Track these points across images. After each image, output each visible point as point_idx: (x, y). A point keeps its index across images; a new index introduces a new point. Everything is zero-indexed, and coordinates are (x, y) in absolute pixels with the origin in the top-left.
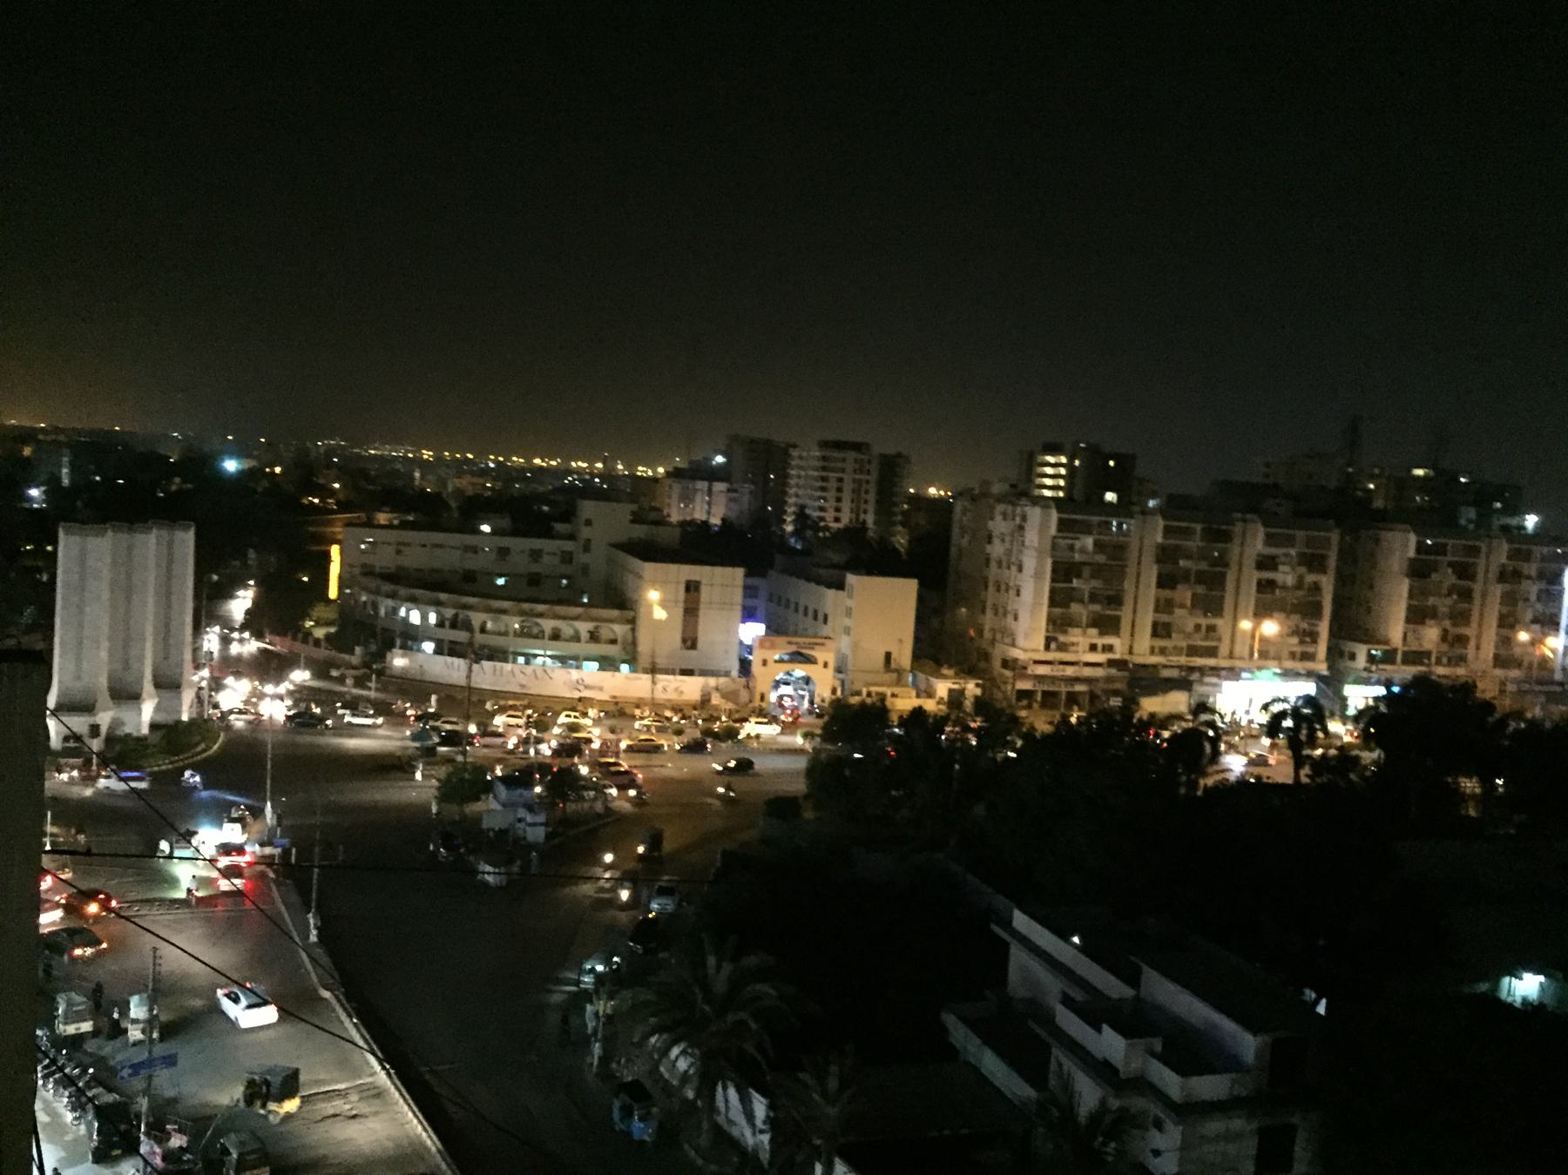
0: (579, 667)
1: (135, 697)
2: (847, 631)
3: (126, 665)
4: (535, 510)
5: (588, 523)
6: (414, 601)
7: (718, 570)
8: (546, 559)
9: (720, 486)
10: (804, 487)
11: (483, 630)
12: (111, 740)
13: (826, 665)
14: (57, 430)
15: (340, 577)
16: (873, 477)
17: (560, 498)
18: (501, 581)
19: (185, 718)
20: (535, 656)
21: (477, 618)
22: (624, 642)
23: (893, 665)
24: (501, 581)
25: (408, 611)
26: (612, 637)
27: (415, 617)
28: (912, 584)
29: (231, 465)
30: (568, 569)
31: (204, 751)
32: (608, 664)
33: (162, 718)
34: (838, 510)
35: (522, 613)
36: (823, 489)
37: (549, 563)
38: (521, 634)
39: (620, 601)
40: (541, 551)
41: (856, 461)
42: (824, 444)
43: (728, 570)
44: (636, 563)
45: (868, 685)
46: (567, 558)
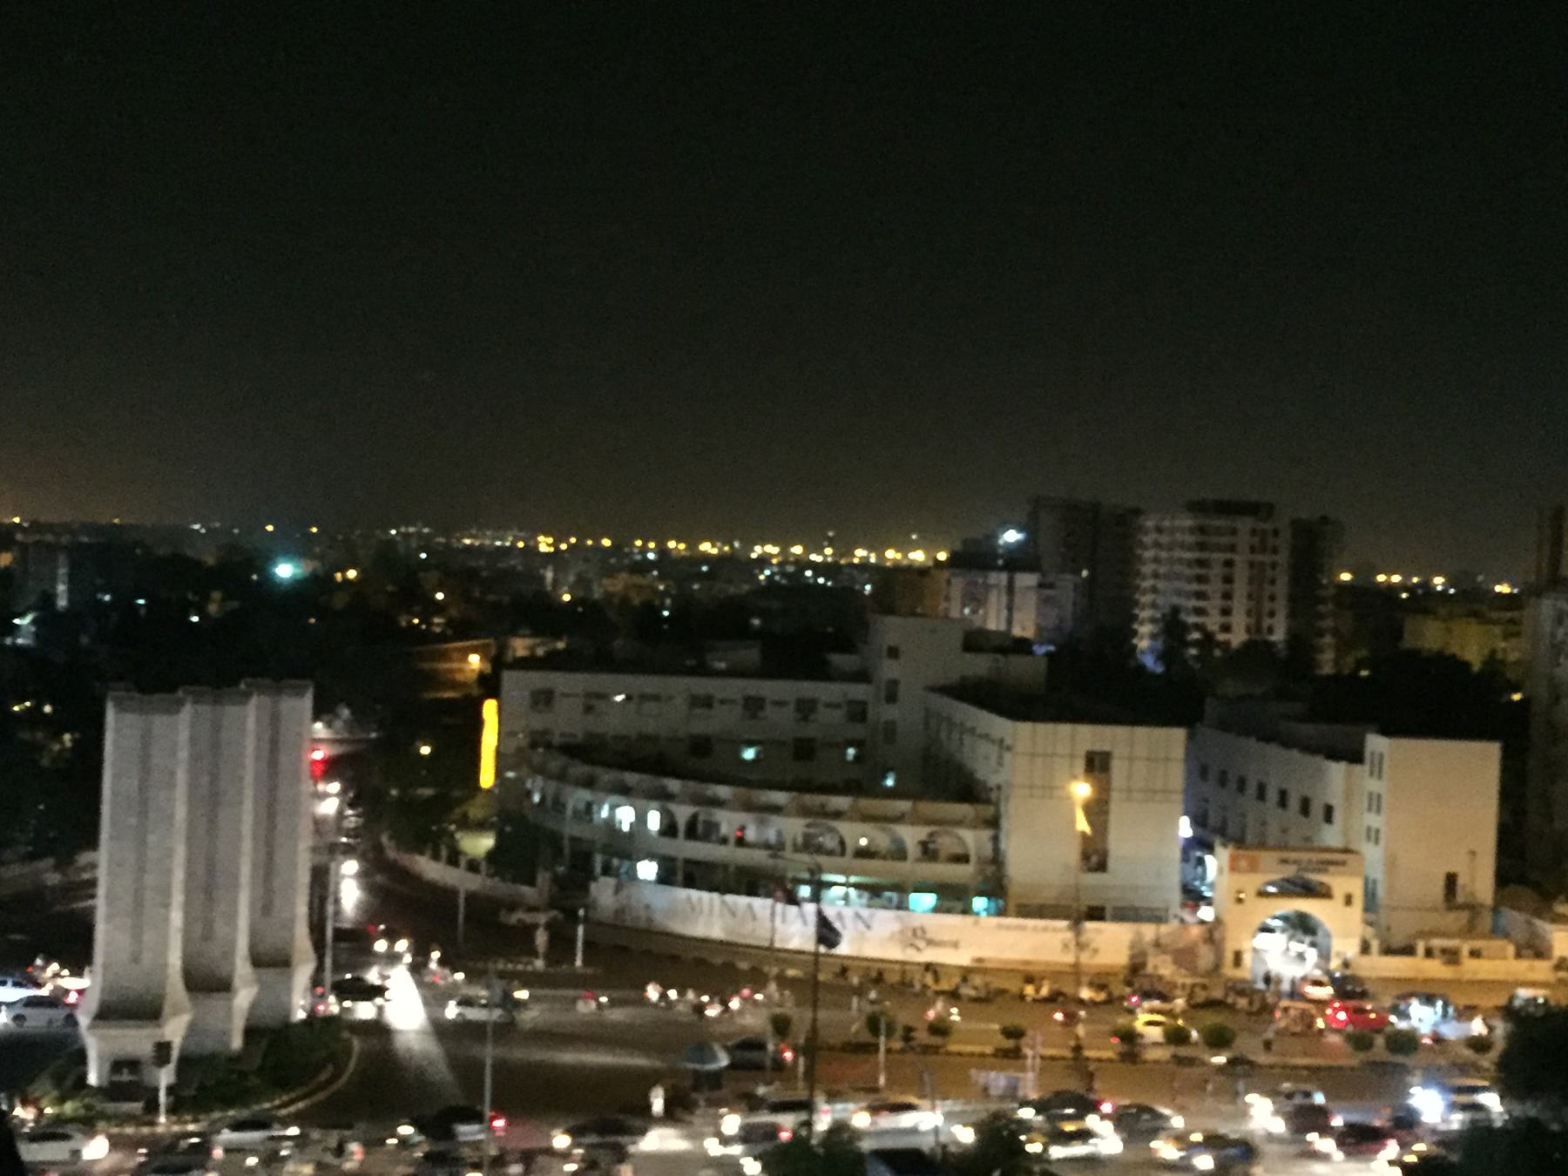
0: (902, 906)
2: (1373, 835)
3: (208, 936)
4: (814, 630)
6: (625, 792)
7: (1141, 732)
9: (1026, 580)
11: (741, 842)
12: (186, 1062)
14: (36, 526)
15: (499, 754)
16: (1283, 558)
17: (776, 605)
18: (749, 754)
19: (301, 1015)
20: (831, 884)
21: (728, 821)
22: (982, 861)
23: (1460, 898)
24: (749, 754)
25: (613, 808)
27: (625, 816)
29: (285, 571)
30: (859, 731)
31: (329, 1082)
32: (953, 898)
34: (1226, 612)
35: (805, 812)
36: (1201, 579)
37: (829, 720)
38: (809, 845)
39: (952, 783)
41: (1254, 532)
42: (1198, 507)
44: (1000, 726)
45: (1423, 934)
46: (858, 712)
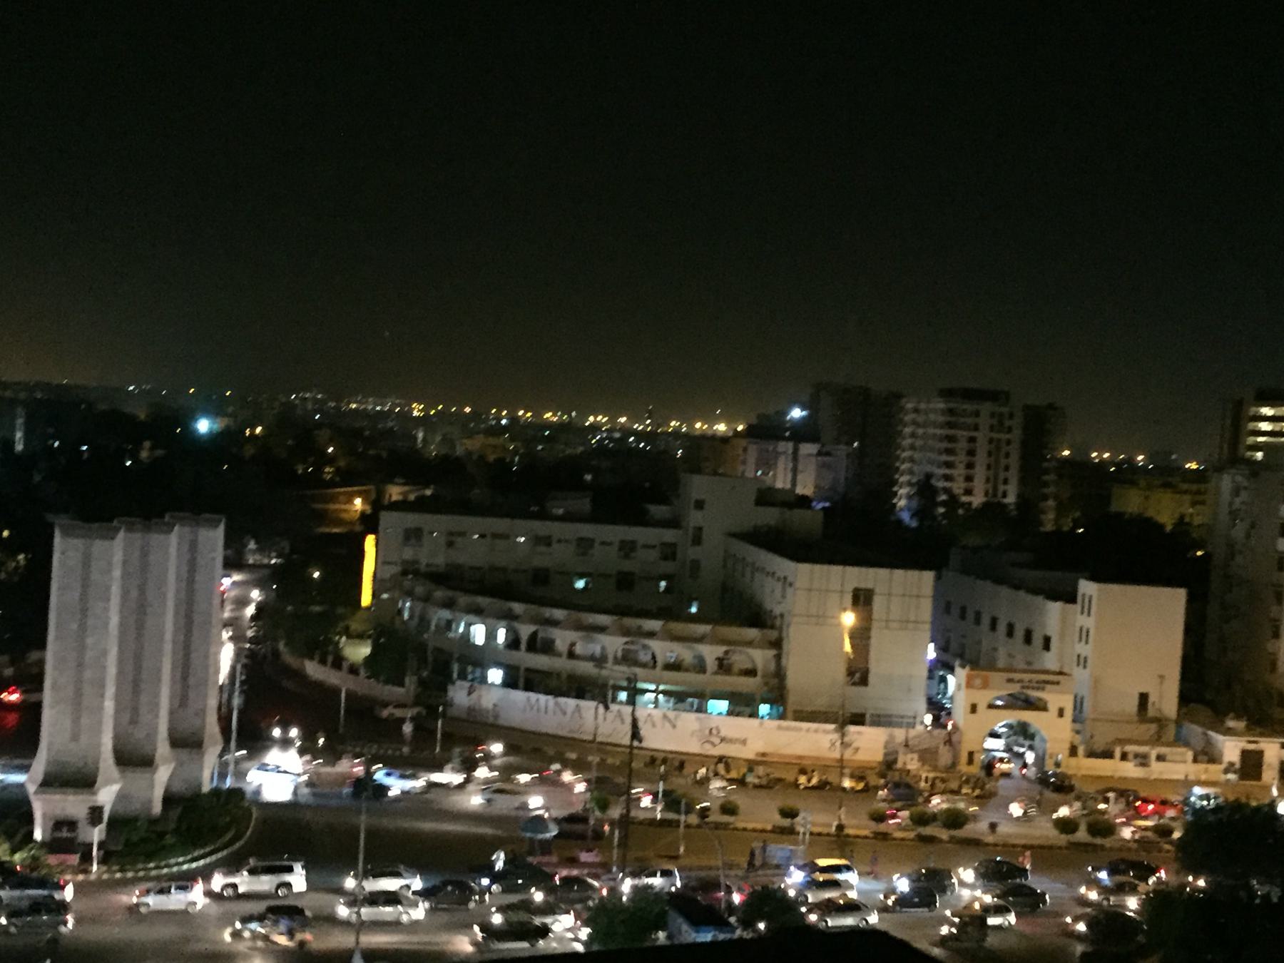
1: (146, 762)
2: (1082, 661)
4: (636, 485)
5: (700, 505)
6: (479, 613)
8: (641, 554)
9: (808, 449)
10: (922, 448)
13: (1061, 713)
16: (1017, 434)
21: (562, 638)
23: (1151, 712)
24: (580, 584)
26: (749, 666)
27: (479, 634)
28: (1180, 595)
29: (203, 426)
30: (669, 567)
33: (178, 787)
35: (626, 632)
36: (949, 452)
39: (744, 611)
40: (633, 543)
41: (992, 415)
42: (947, 394)
43: (913, 575)
46: (669, 552)
